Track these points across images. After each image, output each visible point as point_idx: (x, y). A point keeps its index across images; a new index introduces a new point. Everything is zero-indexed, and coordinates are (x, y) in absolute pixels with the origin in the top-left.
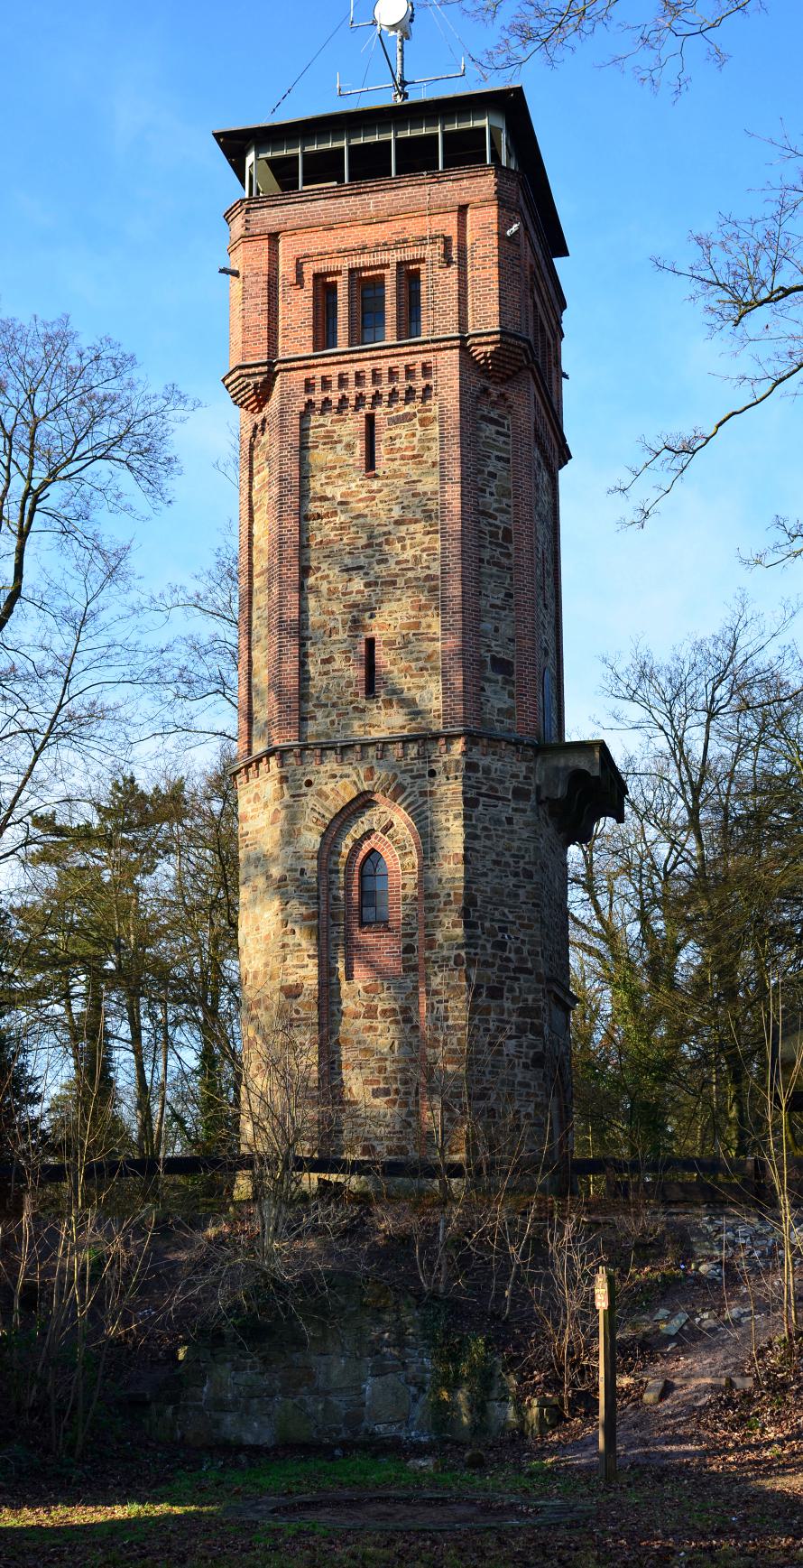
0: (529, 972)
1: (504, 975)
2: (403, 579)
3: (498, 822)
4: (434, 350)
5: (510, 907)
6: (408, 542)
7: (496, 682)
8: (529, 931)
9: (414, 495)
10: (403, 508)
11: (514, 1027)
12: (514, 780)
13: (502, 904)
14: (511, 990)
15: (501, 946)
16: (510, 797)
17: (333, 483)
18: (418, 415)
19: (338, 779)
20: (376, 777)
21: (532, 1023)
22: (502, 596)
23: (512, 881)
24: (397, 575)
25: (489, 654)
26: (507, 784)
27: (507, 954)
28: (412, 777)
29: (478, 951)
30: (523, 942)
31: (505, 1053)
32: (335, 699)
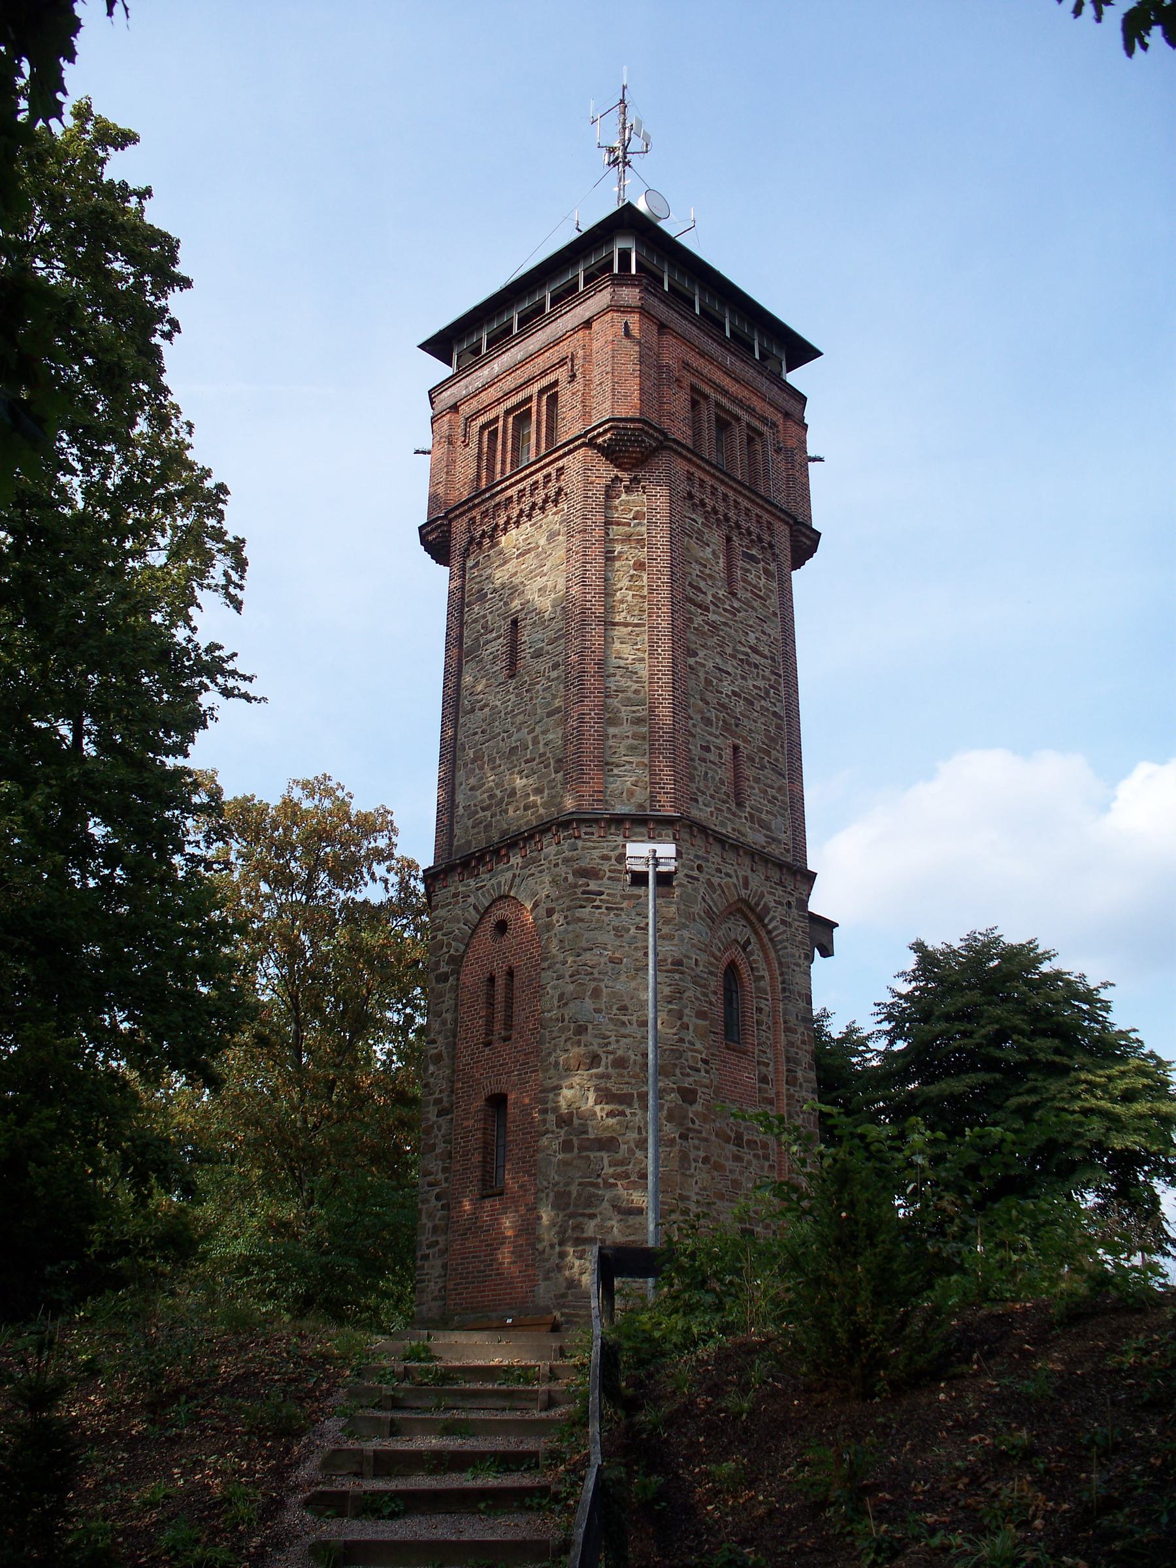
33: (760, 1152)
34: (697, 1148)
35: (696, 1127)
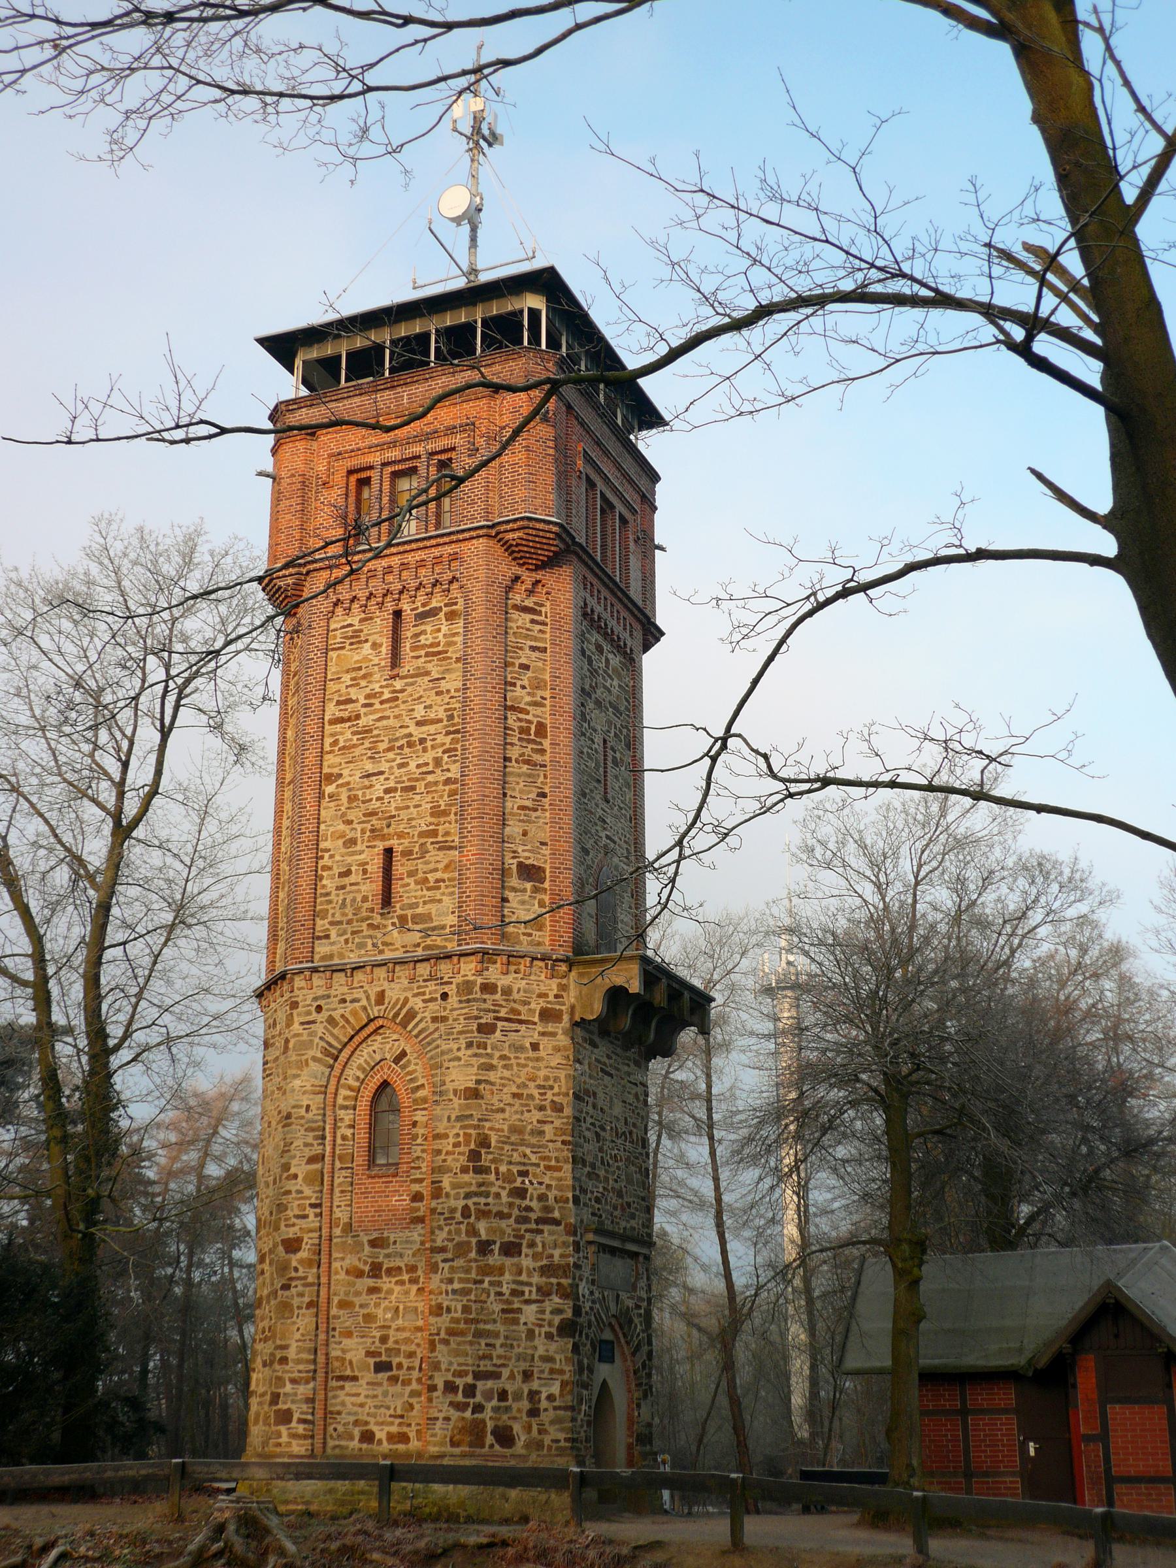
0: (557, 1222)
1: (524, 1227)
2: (423, 783)
3: (521, 1048)
4: (438, 545)
5: (533, 1146)
6: (429, 744)
7: (525, 890)
8: (556, 1174)
9: (437, 694)
10: (425, 707)
11: (534, 1289)
12: (541, 1000)
13: (523, 1143)
14: (532, 1245)
15: (521, 1193)
16: (536, 1019)
17: (358, 684)
18: (445, 609)
19: (348, 1004)
20: (386, 1001)
21: (559, 1284)
22: (533, 796)
23: (537, 1115)
24: (417, 780)
25: (515, 861)
26: (533, 1006)
27: (527, 1202)
28: (424, 1001)
29: (490, 1200)
30: (549, 1187)
31: (522, 1321)
32: (350, 916)
33: (406, 1277)
34: (301, 1295)
35: (300, 1274)
